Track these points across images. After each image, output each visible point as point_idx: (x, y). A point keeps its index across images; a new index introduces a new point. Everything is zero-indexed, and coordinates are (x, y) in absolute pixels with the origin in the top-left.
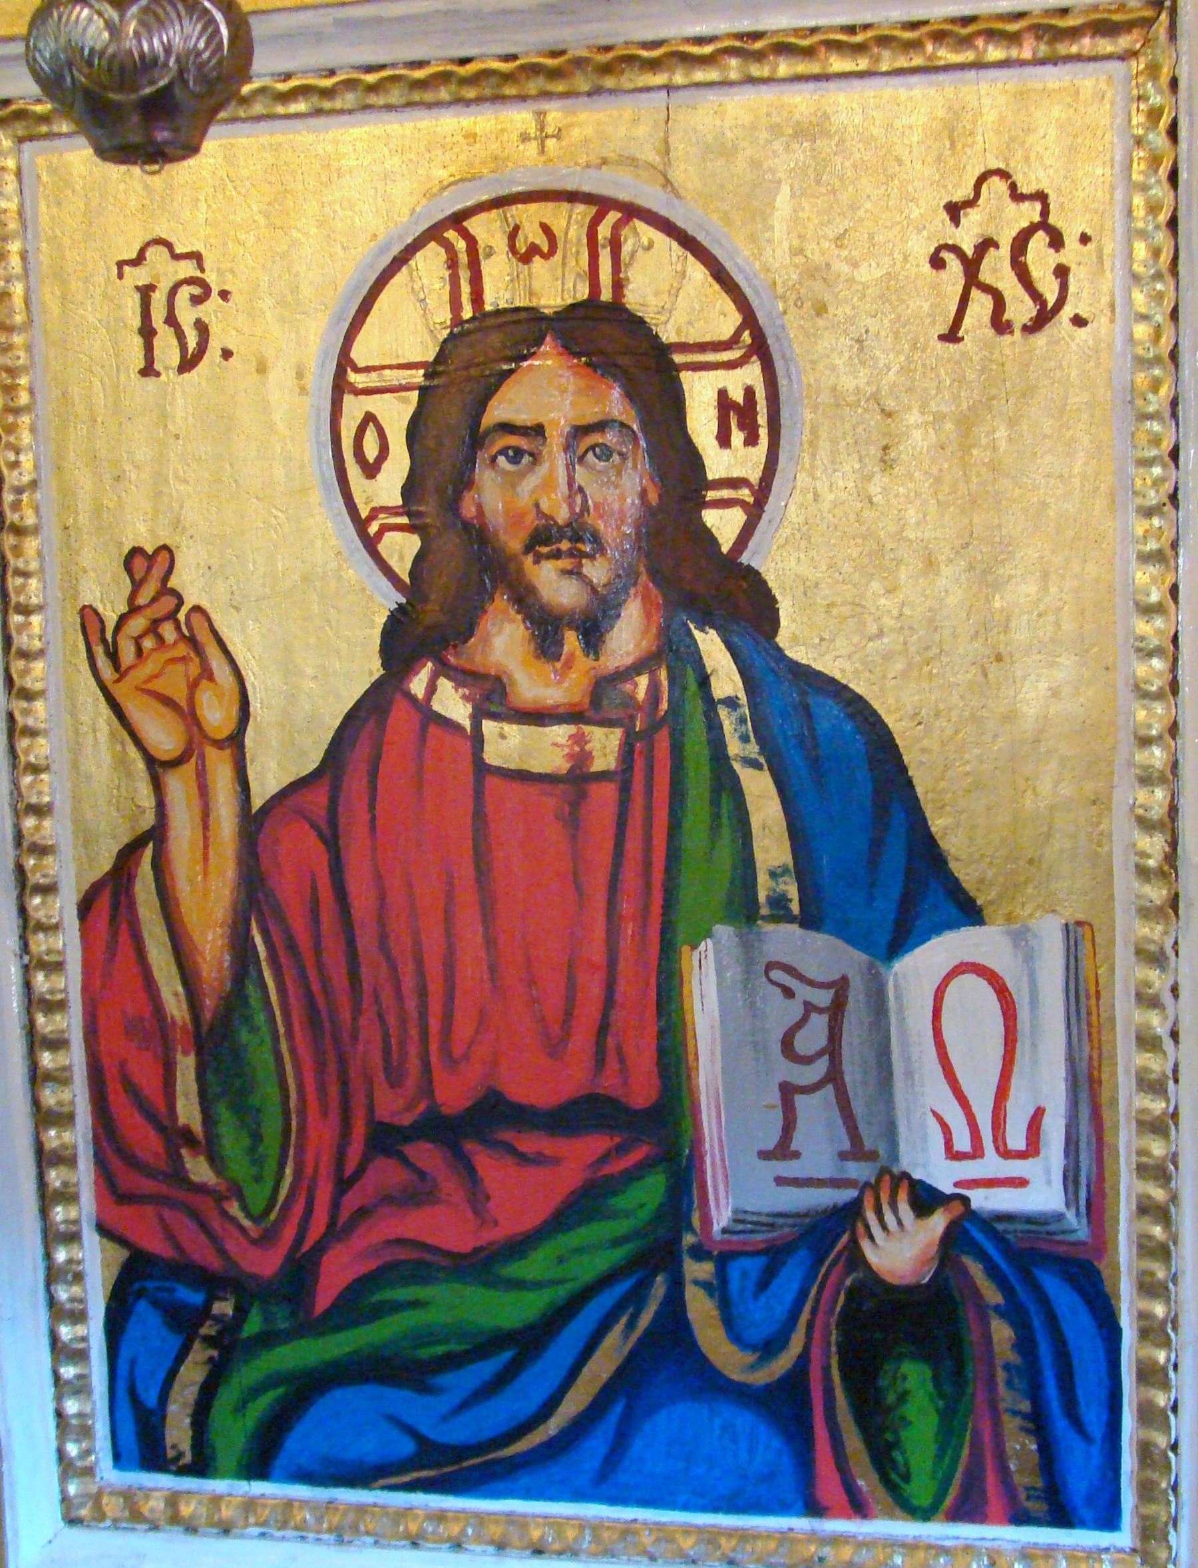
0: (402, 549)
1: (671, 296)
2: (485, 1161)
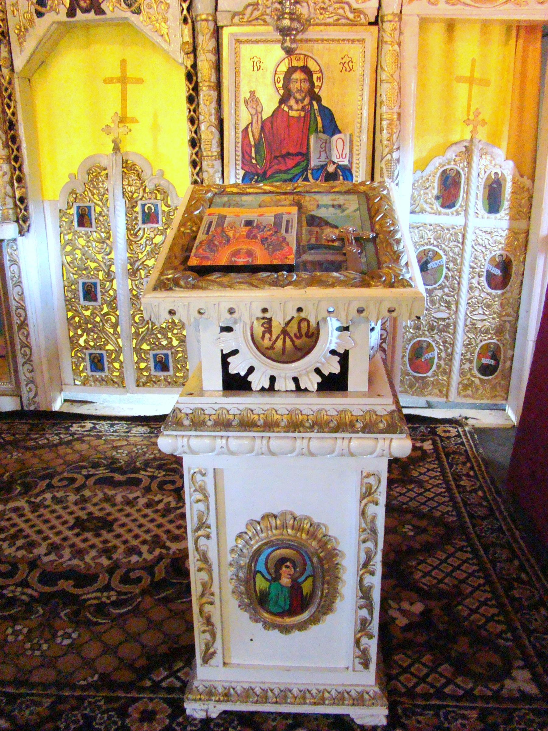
0: (282, 92)
1: (312, 65)
2: (287, 160)
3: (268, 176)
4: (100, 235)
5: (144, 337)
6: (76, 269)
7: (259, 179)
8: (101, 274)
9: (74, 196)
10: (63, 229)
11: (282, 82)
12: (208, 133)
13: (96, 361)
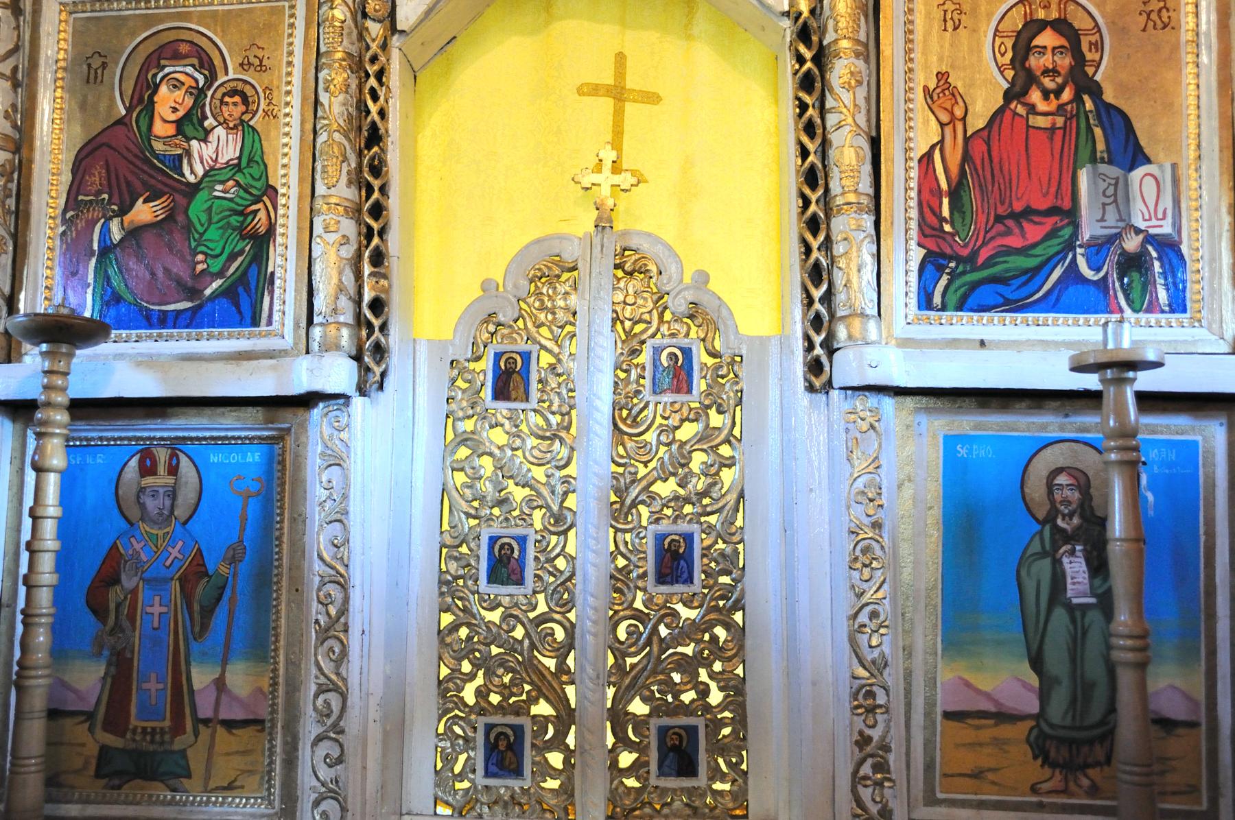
0: (1010, 74)
3: (980, 261)
4: (547, 420)
5: (636, 678)
6: (476, 504)
7: (960, 269)
8: (538, 515)
9: (492, 328)
10: (454, 406)
11: (1009, 55)
12: (848, 151)
13: (502, 745)
